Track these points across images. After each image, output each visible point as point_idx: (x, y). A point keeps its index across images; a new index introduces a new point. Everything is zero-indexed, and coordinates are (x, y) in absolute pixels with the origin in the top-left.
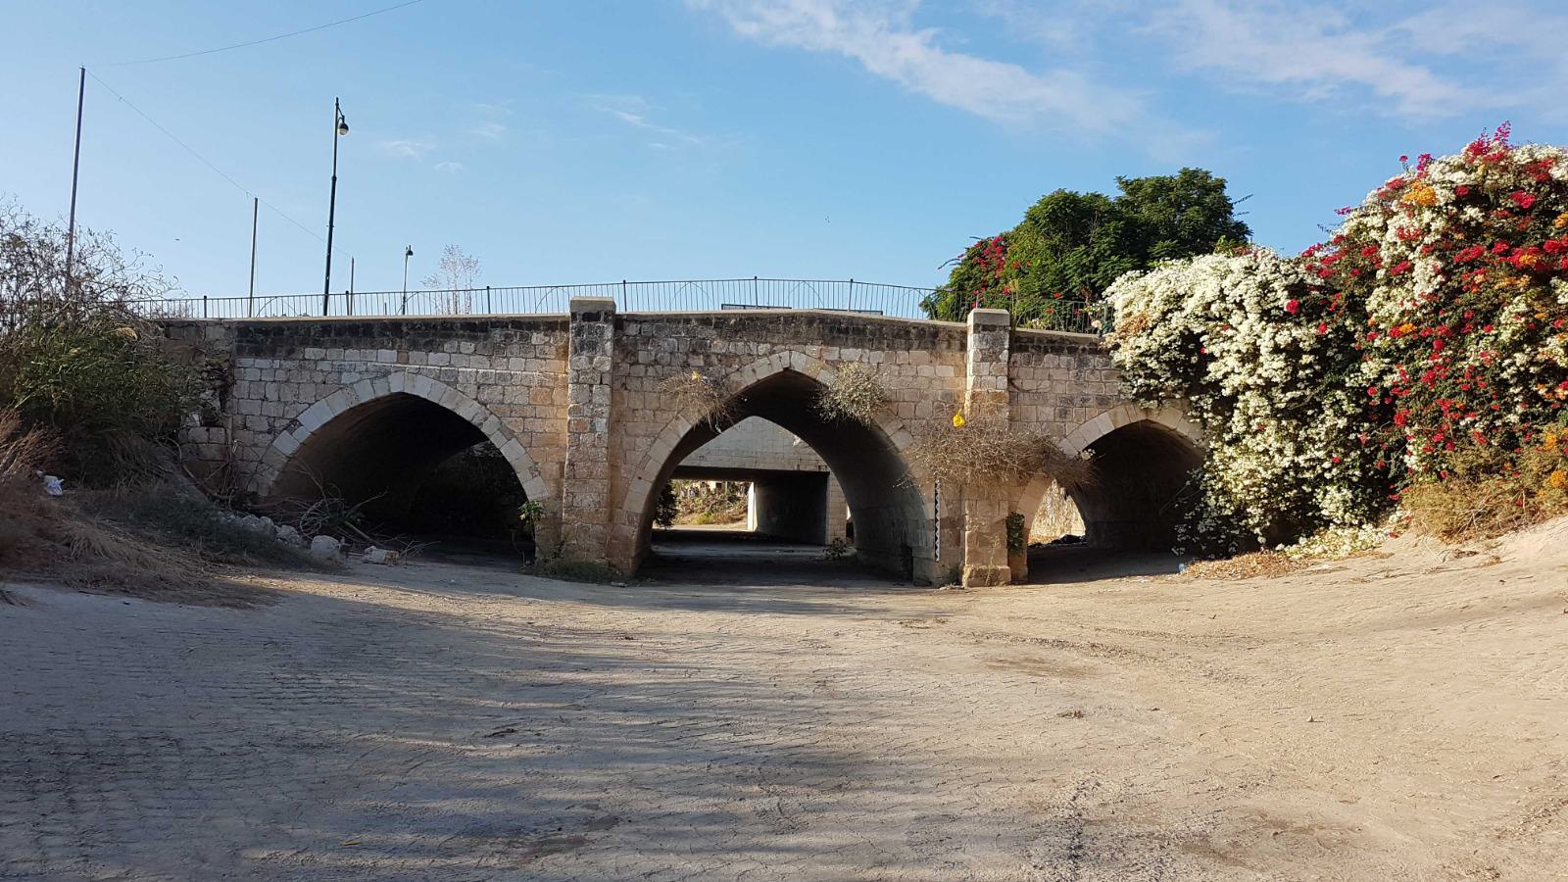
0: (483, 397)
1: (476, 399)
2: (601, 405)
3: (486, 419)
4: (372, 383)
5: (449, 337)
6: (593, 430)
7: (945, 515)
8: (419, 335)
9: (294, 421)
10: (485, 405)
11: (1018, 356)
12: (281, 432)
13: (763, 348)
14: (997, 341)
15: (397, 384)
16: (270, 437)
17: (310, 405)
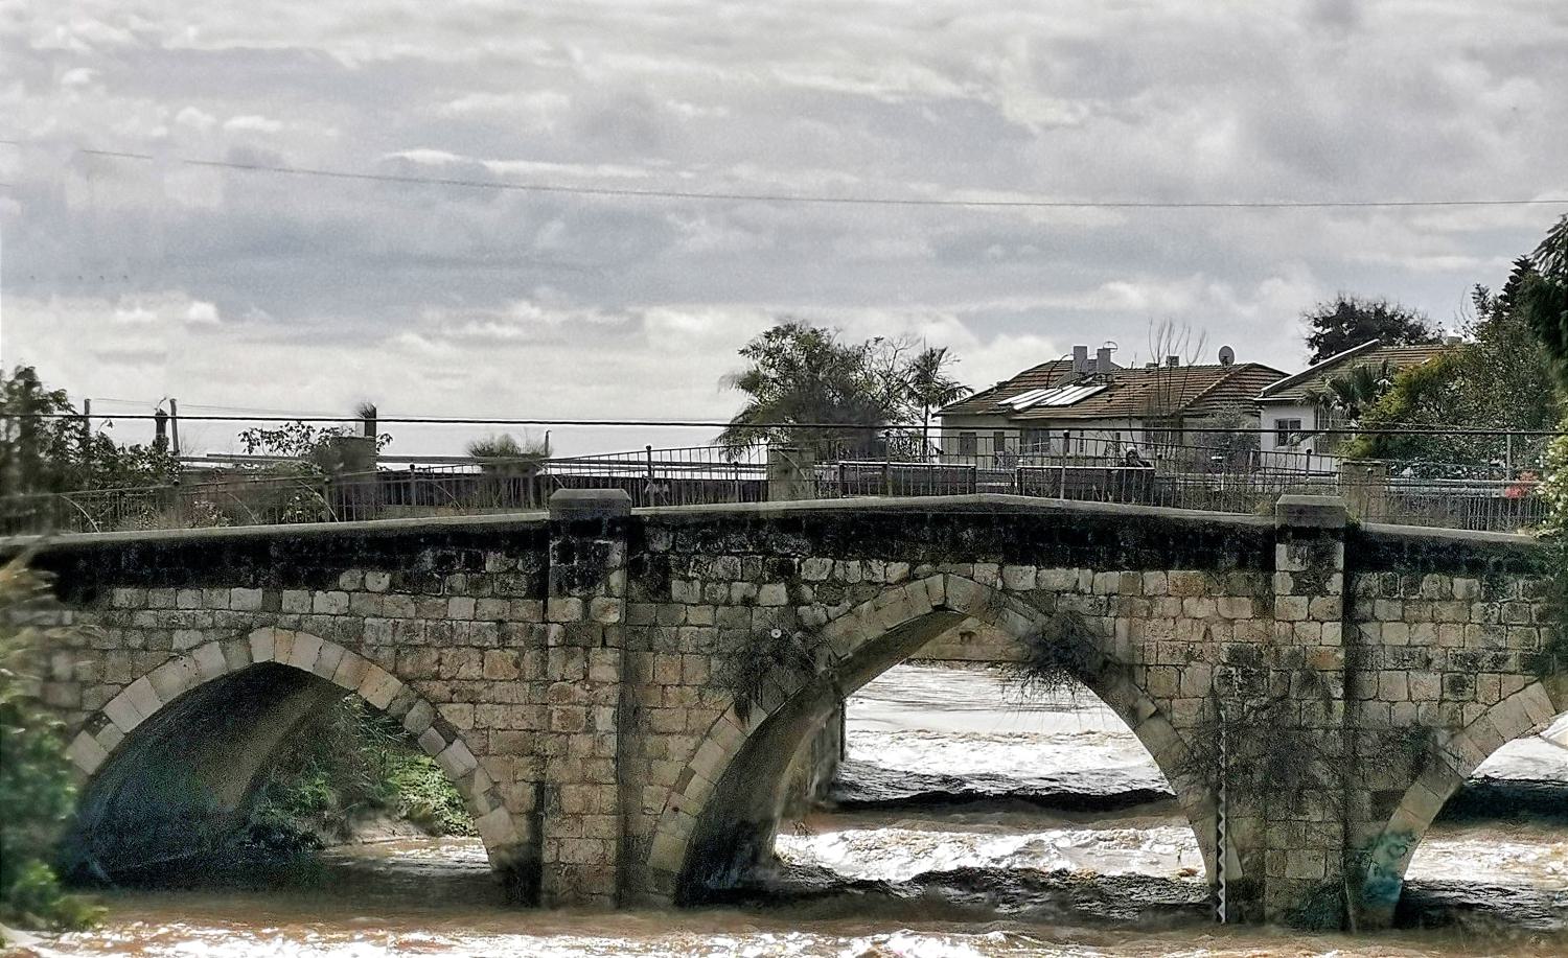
1: (394, 672)
6: (590, 729)
7: (1238, 874)
11: (1370, 580)
12: (78, 732)
13: (898, 569)
14: (1321, 557)
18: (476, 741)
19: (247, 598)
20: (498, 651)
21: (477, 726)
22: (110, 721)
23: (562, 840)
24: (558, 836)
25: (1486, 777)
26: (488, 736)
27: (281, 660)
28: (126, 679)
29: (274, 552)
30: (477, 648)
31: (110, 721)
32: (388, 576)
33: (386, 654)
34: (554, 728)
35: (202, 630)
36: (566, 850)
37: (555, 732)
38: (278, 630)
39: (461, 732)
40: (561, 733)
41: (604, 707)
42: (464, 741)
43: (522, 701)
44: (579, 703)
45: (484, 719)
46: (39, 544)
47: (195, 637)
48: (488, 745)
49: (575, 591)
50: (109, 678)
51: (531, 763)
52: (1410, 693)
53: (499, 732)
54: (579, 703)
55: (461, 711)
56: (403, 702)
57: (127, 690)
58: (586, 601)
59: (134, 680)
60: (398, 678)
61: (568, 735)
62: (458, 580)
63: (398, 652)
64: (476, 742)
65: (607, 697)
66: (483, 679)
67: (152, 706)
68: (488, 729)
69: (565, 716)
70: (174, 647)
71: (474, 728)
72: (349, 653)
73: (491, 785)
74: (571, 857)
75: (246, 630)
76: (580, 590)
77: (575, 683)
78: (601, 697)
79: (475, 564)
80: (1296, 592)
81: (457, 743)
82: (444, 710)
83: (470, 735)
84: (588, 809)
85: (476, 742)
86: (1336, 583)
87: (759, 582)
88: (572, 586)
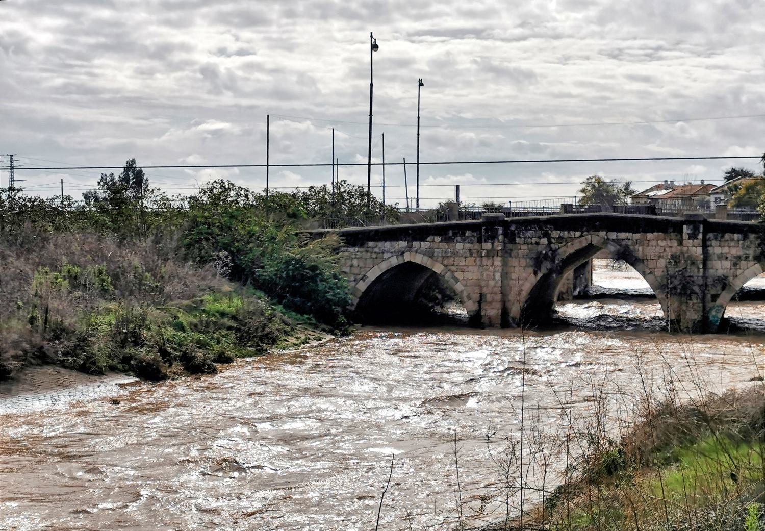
3: (446, 273)
6: (494, 279)
9: (365, 276)
13: (578, 234)
15: (408, 257)
19: (403, 244)
36: (488, 311)
45: (467, 277)
47: (390, 255)
58: (493, 244)
67: (379, 274)
69: (487, 275)
75: (403, 253)
79: (463, 234)
80: (689, 238)
85: (464, 282)
86: (700, 236)
87: (539, 238)
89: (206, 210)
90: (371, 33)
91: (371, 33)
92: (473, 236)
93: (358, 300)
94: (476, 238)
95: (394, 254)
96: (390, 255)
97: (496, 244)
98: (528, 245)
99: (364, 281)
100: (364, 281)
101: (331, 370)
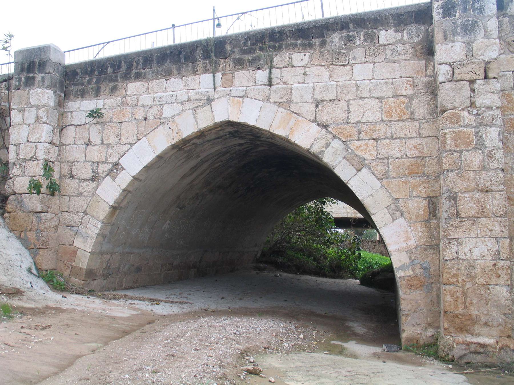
0: (324, 117)
1: (315, 121)
2: (489, 108)
3: (328, 145)
4: (194, 114)
5: (277, 49)
6: (480, 146)
8: (245, 52)
9: (116, 166)
10: (326, 127)
12: (104, 178)
16: (93, 184)
17: (131, 145)
18: (378, 168)
20: (392, 99)
21: (379, 156)
22: (124, 169)
23: (459, 241)
24: (457, 236)
25: (158, 304)
26: (388, 163)
27: (234, 118)
28: (133, 140)
29: (229, 48)
30: (376, 98)
31: (124, 169)
32: (308, 55)
33: (308, 109)
34: (448, 147)
35: (181, 103)
36: (465, 248)
37: (450, 151)
38: (231, 98)
39: (367, 162)
40: (455, 151)
41: (491, 127)
42: (370, 169)
43: (414, 135)
44: (469, 125)
45: (384, 152)
46: (238, 148)
47: (176, 108)
48: (388, 170)
49: (459, 38)
50: (124, 140)
51: (423, 183)
52: (102, 141)
53: (397, 160)
54: (469, 125)
55: (366, 145)
56: (323, 142)
57: (134, 147)
58: (469, 45)
59: (138, 140)
60: (318, 125)
61: (461, 152)
62: (359, 53)
63: (317, 106)
64: (380, 168)
65: (493, 119)
66: (382, 121)
68: (387, 158)
69: (457, 136)
70: (163, 116)
71: (377, 158)
72: (281, 110)
73: (391, 201)
74: (468, 254)
76: (463, 36)
77: (463, 110)
78: (488, 119)
79: (372, 38)
81: (364, 170)
82: (353, 145)
83: (374, 164)
84: (482, 212)
85: (380, 168)
88: (454, 33)
89: (426, 353)
90: (214, 7)
91: (214, 7)
92: (401, 41)
93: (100, 225)
94: (407, 46)
95: (188, 105)
96: (176, 108)
97: (479, 41)
98: (169, 364)
99: (114, 178)
100: (114, 178)
101: (466, 190)
